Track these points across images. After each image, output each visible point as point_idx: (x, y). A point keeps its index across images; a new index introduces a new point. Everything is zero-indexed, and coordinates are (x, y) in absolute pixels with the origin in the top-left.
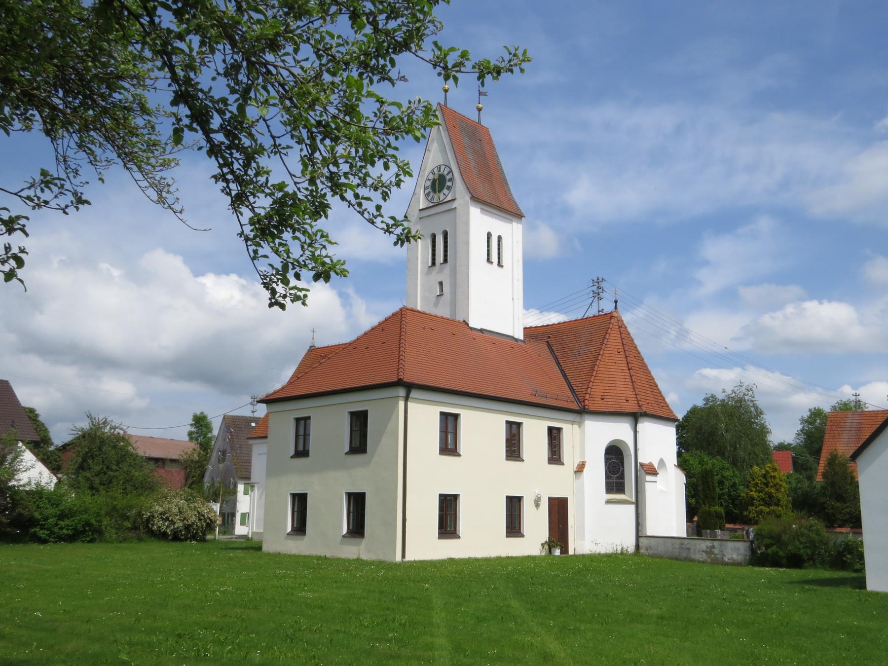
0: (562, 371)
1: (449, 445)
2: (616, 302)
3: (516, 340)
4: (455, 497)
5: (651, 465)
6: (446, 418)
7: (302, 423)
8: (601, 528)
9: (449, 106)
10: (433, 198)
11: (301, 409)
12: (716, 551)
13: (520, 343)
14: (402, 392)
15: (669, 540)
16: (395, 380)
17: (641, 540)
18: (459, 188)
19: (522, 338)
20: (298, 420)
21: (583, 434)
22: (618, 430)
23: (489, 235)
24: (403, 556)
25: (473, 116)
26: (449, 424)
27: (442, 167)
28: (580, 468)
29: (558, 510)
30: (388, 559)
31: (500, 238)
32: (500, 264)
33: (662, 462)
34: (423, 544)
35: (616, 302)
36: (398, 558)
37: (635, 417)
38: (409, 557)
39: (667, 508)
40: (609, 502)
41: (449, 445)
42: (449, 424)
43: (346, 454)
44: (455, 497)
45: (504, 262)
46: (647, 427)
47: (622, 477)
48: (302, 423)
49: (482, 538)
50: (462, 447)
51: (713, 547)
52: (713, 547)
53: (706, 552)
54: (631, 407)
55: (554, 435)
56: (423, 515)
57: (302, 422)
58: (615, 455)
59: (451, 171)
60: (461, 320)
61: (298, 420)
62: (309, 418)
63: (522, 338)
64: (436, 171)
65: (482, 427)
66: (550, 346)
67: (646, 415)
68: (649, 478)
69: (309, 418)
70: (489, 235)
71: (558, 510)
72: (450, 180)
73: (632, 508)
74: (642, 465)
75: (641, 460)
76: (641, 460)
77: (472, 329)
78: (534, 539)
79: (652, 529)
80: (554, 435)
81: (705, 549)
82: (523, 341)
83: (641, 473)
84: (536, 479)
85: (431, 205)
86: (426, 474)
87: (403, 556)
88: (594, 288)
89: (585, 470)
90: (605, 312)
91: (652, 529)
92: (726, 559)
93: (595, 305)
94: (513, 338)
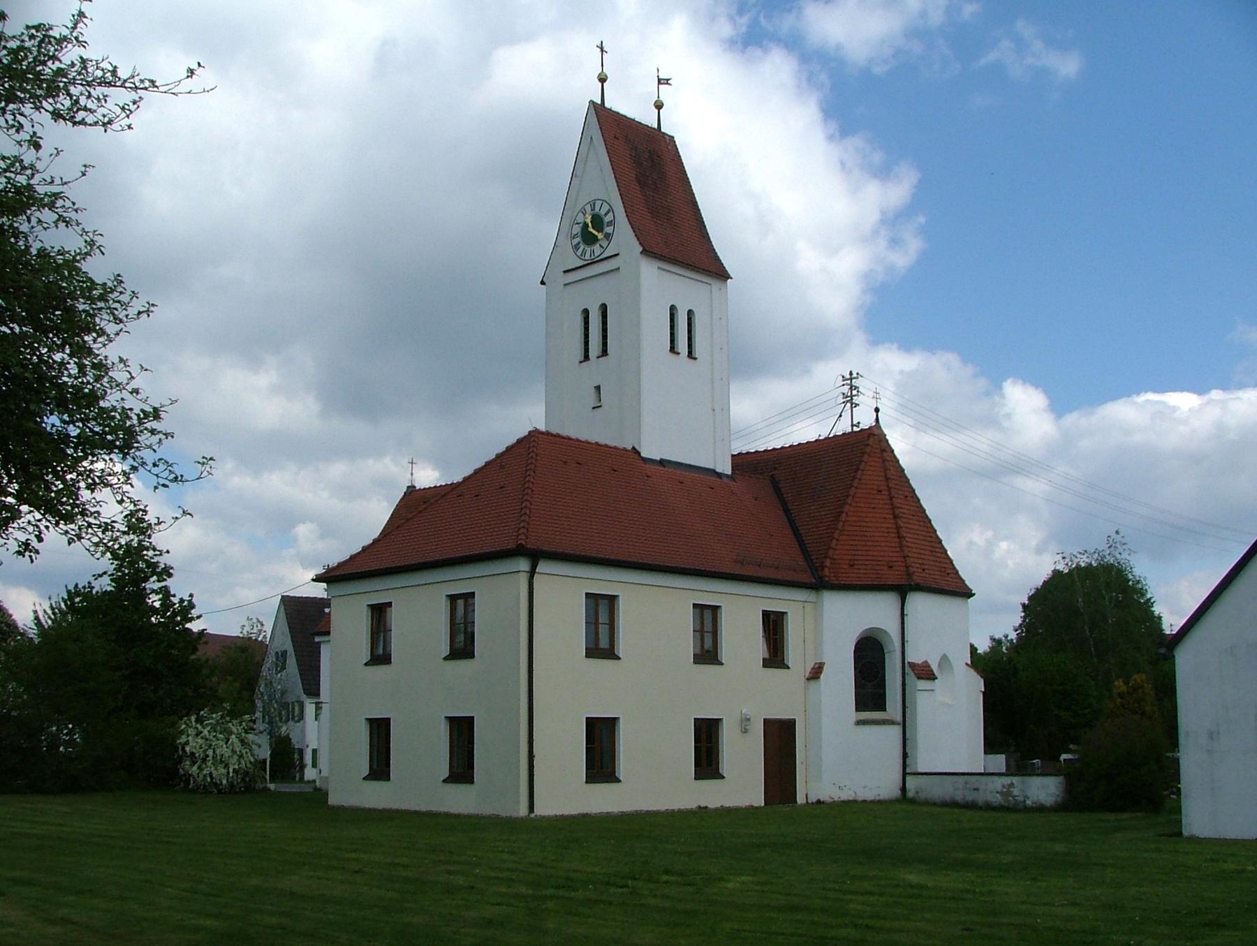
0: (792, 523)
1: (601, 647)
2: (877, 410)
3: (719, 475)
4: (612, 722)
5: (926, 665)
6: (597, 605)
7: (379, 612)
8: (847, 762)
9: (607, 105)
10: (584, 253)
11: (377, 590)
12: (1015, 792)
13: (725, 480)
14: (523, 565)
15: (961, 779)
16: (512, 546)
17: (908, 778)
18: (624, 238)
19: (729, 472)
20: (453, 598)
21: (818, 618)
22: (874, 612)
23: (673, 309)
24: (531, 808)
25: (647, 117)
26: (601, 610)
27: (598, 204)
28: (816, 673)
29: (780, 739)
30: (514, 815)
31: (690, 313)
32: (690, 355)
33: (944, 660)
34: (565, 791)
35: (877, 410)
36: (523, 811)
37: (902, 591)
38: (540, 810)
39: (951, 730)
40: (860, 723)
41: (601, 647)
42: (601, 610)
43: (445, 659)
44: (612, 722)
45: (697, 353)
46: (920, 604)
47: (882, 685)
48: (379, 612)
49: (654, 779)
50: (623, 646)
51: (1012, 784)
52: (1012, 784)
53: (1001, 793)
54: (892, 577)
55: (773, 625)
56: (563, 749)
57: (460, 602)
58: (869, 654)
59: (611, 210)
60: (630, 448)
61: (453, 598)
62: (390, 604)
63: (729, 472)
64: (588, 208)
65: (656, 611)
66: (775, 483)
67: (919, 588)
68: (922, 684)
69: (390, 604)
70: (673, 309)
71: (780, 739)
72: (611, 223)
73: (896, 731)
74: (912, 665)
75: (910, 658)
76: (910, 658)
77: (645, 460)
78: (742, 783)
79: (925, 760)
80: (773, 625)
81: (999, 788)
82: (732, 477)
83: (911, 677)
84: (744, 693)
85: (581, 263)
86: (571, 690)
87: (531, 808)
88: (846, 389)
89: (822, 676)
90: (862, 426)
91: (925, 760)
92: (1028, 802)
93: (847, 415)
94: (714, 471)
